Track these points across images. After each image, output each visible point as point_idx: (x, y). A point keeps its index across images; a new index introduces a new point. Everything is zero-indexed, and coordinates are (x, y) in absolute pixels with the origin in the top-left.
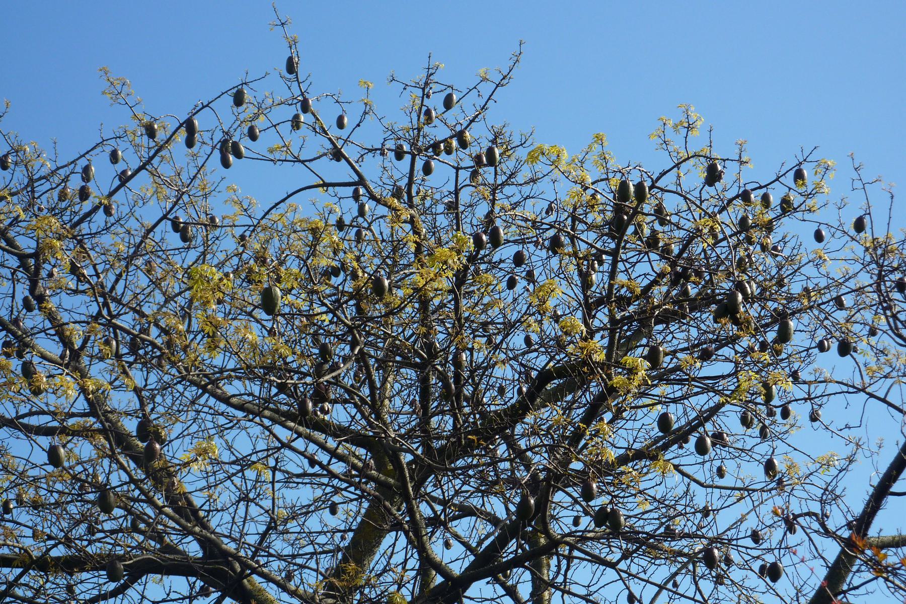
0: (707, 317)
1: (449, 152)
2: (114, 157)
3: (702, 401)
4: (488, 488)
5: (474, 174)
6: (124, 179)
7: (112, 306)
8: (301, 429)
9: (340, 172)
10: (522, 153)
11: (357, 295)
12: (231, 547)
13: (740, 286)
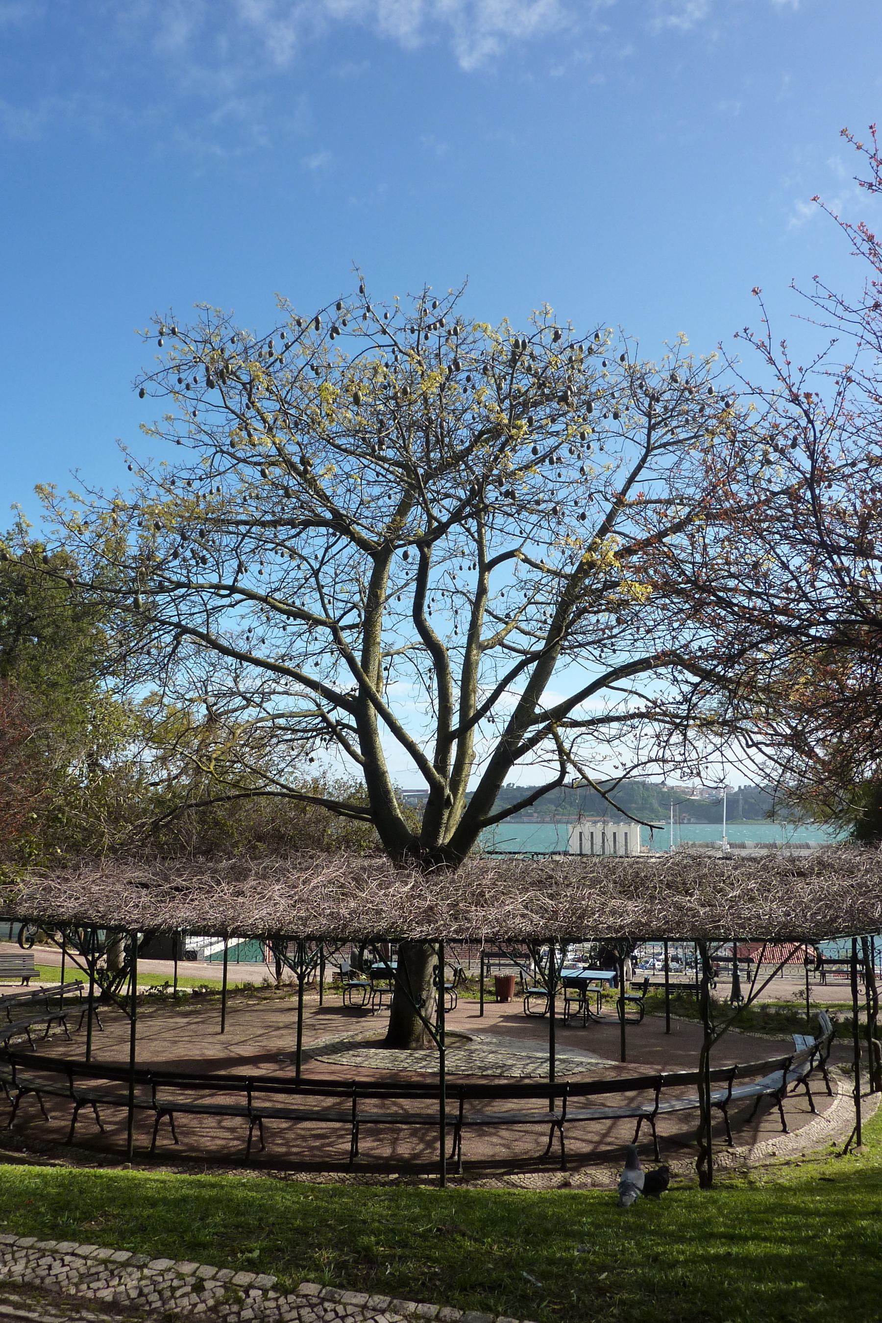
0: (555, 405)
1: (435, 329)
2: (282, 336)
3: (552, 441)
4: (457, 485)
5: (447, 339)
6: (287, 347)
7: (286, 406)
8: (373, 460)
9: (385, 340)
10: (469, 329)
11: (395, 398)
12: (344, 512)
13: (569, 388)
